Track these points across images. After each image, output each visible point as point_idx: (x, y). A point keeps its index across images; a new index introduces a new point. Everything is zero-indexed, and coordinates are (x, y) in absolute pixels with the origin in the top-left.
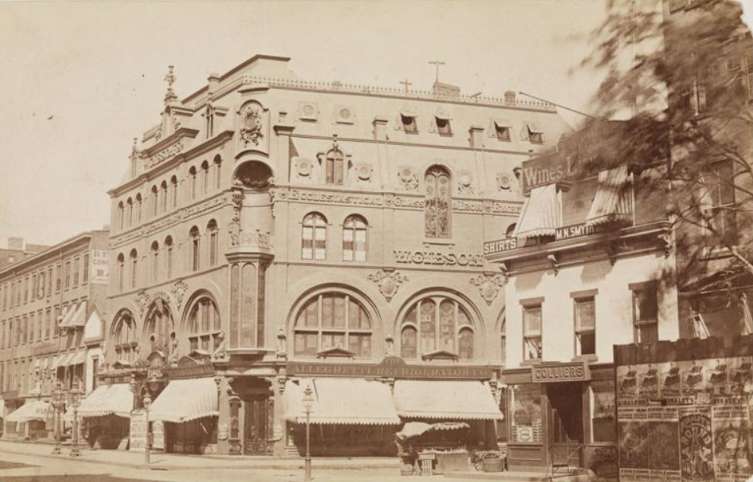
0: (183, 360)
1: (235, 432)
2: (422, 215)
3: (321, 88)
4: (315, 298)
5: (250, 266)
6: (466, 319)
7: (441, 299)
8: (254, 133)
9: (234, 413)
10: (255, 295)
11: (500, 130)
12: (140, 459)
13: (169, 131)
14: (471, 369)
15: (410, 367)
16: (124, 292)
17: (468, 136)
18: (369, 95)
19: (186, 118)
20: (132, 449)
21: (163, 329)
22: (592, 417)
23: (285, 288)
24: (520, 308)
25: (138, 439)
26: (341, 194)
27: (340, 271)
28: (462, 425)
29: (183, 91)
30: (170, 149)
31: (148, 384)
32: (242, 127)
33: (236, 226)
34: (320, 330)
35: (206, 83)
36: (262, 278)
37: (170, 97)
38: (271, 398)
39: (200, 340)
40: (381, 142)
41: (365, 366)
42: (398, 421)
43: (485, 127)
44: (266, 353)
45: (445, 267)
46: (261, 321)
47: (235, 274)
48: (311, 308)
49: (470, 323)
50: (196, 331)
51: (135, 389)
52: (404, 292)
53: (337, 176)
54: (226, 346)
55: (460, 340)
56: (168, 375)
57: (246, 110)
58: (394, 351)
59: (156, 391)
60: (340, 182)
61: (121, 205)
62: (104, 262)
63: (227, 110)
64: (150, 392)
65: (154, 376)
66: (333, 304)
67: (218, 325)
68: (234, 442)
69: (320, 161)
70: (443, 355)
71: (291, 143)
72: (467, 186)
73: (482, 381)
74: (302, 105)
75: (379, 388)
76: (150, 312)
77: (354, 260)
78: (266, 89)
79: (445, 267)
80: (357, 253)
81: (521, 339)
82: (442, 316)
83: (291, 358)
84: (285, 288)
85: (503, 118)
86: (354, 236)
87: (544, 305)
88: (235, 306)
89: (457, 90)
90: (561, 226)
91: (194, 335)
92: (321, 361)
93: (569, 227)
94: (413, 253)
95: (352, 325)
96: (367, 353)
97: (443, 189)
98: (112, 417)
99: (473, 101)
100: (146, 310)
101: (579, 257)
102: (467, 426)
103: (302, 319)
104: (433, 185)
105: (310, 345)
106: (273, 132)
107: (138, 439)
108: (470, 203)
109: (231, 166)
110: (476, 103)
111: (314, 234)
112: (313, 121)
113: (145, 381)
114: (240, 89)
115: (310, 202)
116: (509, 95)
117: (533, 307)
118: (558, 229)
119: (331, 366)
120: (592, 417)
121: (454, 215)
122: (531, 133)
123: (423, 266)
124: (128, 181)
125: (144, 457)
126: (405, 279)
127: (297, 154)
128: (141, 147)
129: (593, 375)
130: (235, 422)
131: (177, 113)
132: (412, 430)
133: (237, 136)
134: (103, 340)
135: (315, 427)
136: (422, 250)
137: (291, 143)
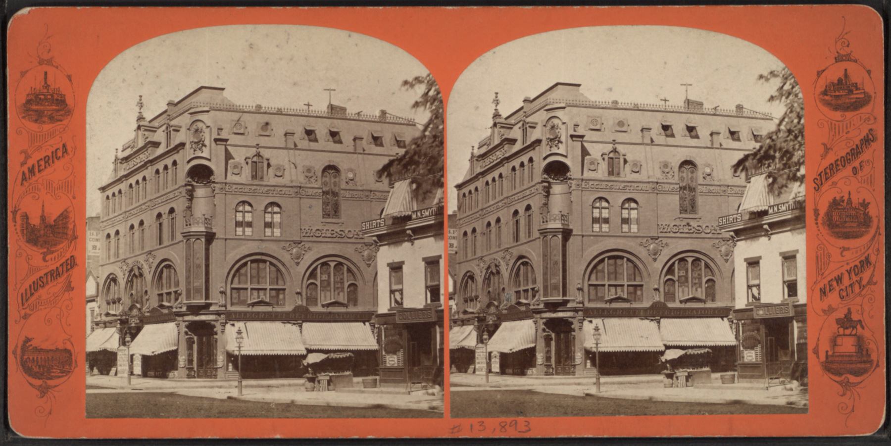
0: (154, 310)
1: (190, 361)
2: (677, 197)
3: (604, 105)
4: (245, 264)
5: (555, 238)
6: (710, 273)
7: (335, 263)
8: (555, 140)
9: (190, 348)
10: (560, 259)
11: (732, 133)
12: (125, 383)
13: (141, 143)
14: (714, 309)
15: (313, 313)
16: (469, 258)
17: (710, 138)
18: (282, 114)
19: (508, 131)
20: (119, 375)
21: (139, 288)
22: (796, 342)
23: (223, 258)
24: (745, 264)
25: (123, 368)
26: (619, 184)
27: (619, 240)
28: (348, 354)
29: (505, 112)
30: (141, 156)
31: (487, 326)
32: (548, 136)
33: (189, 212)
34: (607, 283)
35: (522, 104)
36: (207, 250)
37: (496, 115)
38: (573, 333)
39: (165, 295)
40: (647, 144)
41: (639, 309)
42: (305, 352)
43: (722, 131)
44: (210, 304)
45: (694, 235)
46: (564, 278)
47: (188, 247)
48: (243, 271)
49: (713, 276)
50: (519, 286)
51: (121, 331)
52: (308, 258)
53: (616, 171)
54: (183, 299)
55: (706, 288)
56: (144, 321)
57: (194, 126)
58: (659, 298)
59: (134, 333)
60: (262, 178)
61: (108, 198)
62: (454, 238)
63: (536, 124)
64: (488, 331)
65: (133, 322)
66: (258, 267)
67: (534, 282)
68: (548, 366)
69: (247, 163)
70: (618, 299)
71: (226, 150)
72: (709, 175)
73: (722, 318)
74: (590, 119)
75: (291, 329)
76: (486, 273)
77: (630, 231)
78: (564, 108)
79: (694, 235)
80: (275, 230)
81: (746, 287)
82: (692, 270)
83: (587, 305)
84: (223, 258)
85: (377, 129)
86: (272, 218)
87: (761, 262)
88: (188, 270)
89: (701, 104)
90: (772, 204)
91: (526, 288)
92: (250, 309)
93: (421, 211)
94: (671, 225)
95: (629, 279)
96: (641, 300)
97: (692, 178)
98: (105, 352)
99: (356, 117)
100: (484, 272)
101: (786, 227)
102: (710, 351)
103: (593, 276)
104: (327, 179)
105: (599, 295)
106: (213, 144)
107: (123, 368)
108: (355, 193)
109: (184, 169)
110: (358, 118)
111: (601, 213)
112: (242, 134)
113: (484, 324)
114: (547, 108)
115: (598, 190)
116: (739, 107)
117: (753, 263)
118: (770, 207)
119: (615, 310)
120: (796, 342)
121: (700, 197)
122: (755, 136)
123: (678, 235)
124: (468, 178)
125: (484, 377)
126: (667, 244)
127: (589, 155)
128: (121, 155)
129: (796, 312)
130: (548, 352)
131: (146, 130)
132: (313, 359)
133: (544, 143)
134: (97, 296)
135: (244, 357)
136: (678, 223)
137: (226, 150)
